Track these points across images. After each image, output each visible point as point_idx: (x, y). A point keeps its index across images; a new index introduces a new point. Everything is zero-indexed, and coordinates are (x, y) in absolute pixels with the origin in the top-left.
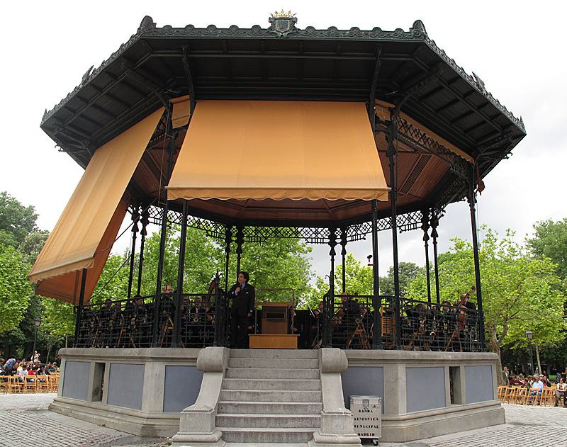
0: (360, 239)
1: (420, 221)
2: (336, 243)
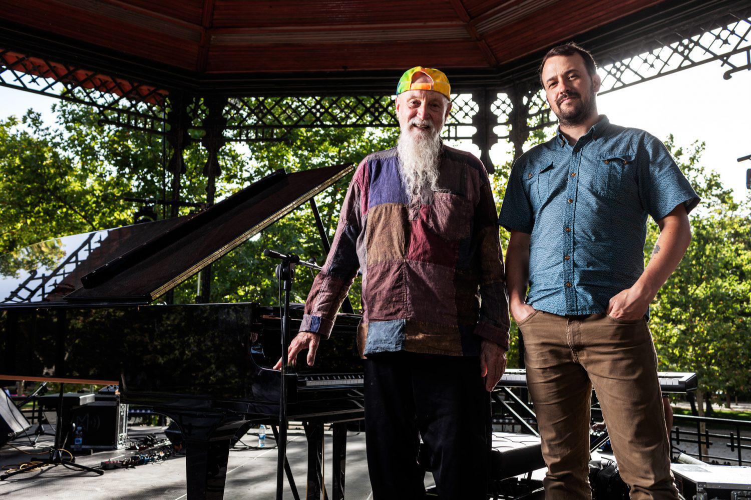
1: (469, 120)
2: (495, 139)
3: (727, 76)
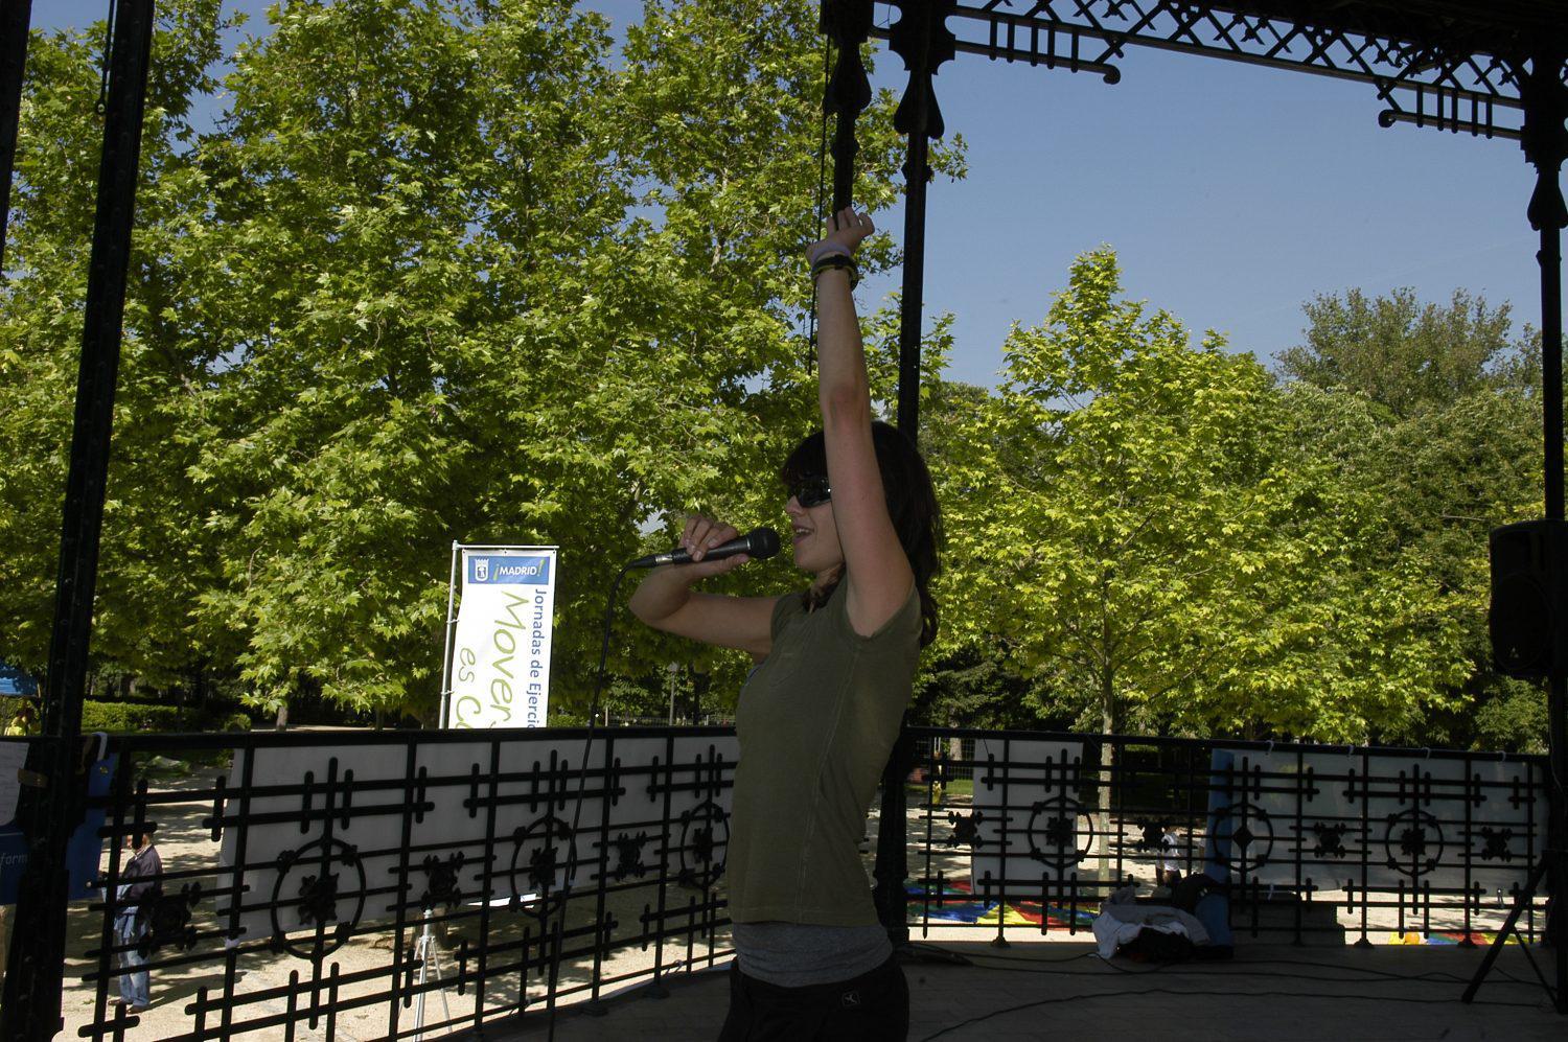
0: (1075, 63)
3: (1385, 120)
